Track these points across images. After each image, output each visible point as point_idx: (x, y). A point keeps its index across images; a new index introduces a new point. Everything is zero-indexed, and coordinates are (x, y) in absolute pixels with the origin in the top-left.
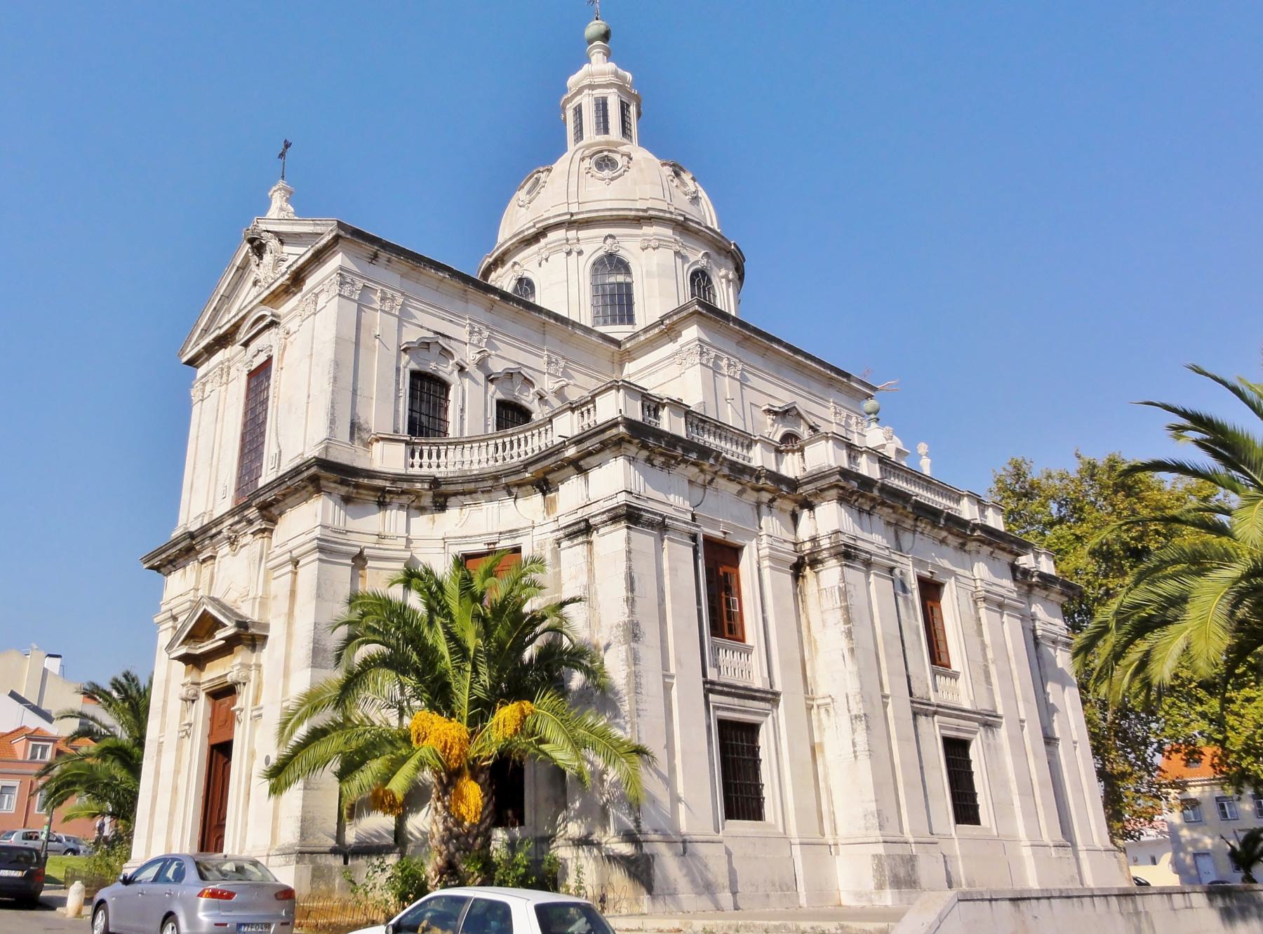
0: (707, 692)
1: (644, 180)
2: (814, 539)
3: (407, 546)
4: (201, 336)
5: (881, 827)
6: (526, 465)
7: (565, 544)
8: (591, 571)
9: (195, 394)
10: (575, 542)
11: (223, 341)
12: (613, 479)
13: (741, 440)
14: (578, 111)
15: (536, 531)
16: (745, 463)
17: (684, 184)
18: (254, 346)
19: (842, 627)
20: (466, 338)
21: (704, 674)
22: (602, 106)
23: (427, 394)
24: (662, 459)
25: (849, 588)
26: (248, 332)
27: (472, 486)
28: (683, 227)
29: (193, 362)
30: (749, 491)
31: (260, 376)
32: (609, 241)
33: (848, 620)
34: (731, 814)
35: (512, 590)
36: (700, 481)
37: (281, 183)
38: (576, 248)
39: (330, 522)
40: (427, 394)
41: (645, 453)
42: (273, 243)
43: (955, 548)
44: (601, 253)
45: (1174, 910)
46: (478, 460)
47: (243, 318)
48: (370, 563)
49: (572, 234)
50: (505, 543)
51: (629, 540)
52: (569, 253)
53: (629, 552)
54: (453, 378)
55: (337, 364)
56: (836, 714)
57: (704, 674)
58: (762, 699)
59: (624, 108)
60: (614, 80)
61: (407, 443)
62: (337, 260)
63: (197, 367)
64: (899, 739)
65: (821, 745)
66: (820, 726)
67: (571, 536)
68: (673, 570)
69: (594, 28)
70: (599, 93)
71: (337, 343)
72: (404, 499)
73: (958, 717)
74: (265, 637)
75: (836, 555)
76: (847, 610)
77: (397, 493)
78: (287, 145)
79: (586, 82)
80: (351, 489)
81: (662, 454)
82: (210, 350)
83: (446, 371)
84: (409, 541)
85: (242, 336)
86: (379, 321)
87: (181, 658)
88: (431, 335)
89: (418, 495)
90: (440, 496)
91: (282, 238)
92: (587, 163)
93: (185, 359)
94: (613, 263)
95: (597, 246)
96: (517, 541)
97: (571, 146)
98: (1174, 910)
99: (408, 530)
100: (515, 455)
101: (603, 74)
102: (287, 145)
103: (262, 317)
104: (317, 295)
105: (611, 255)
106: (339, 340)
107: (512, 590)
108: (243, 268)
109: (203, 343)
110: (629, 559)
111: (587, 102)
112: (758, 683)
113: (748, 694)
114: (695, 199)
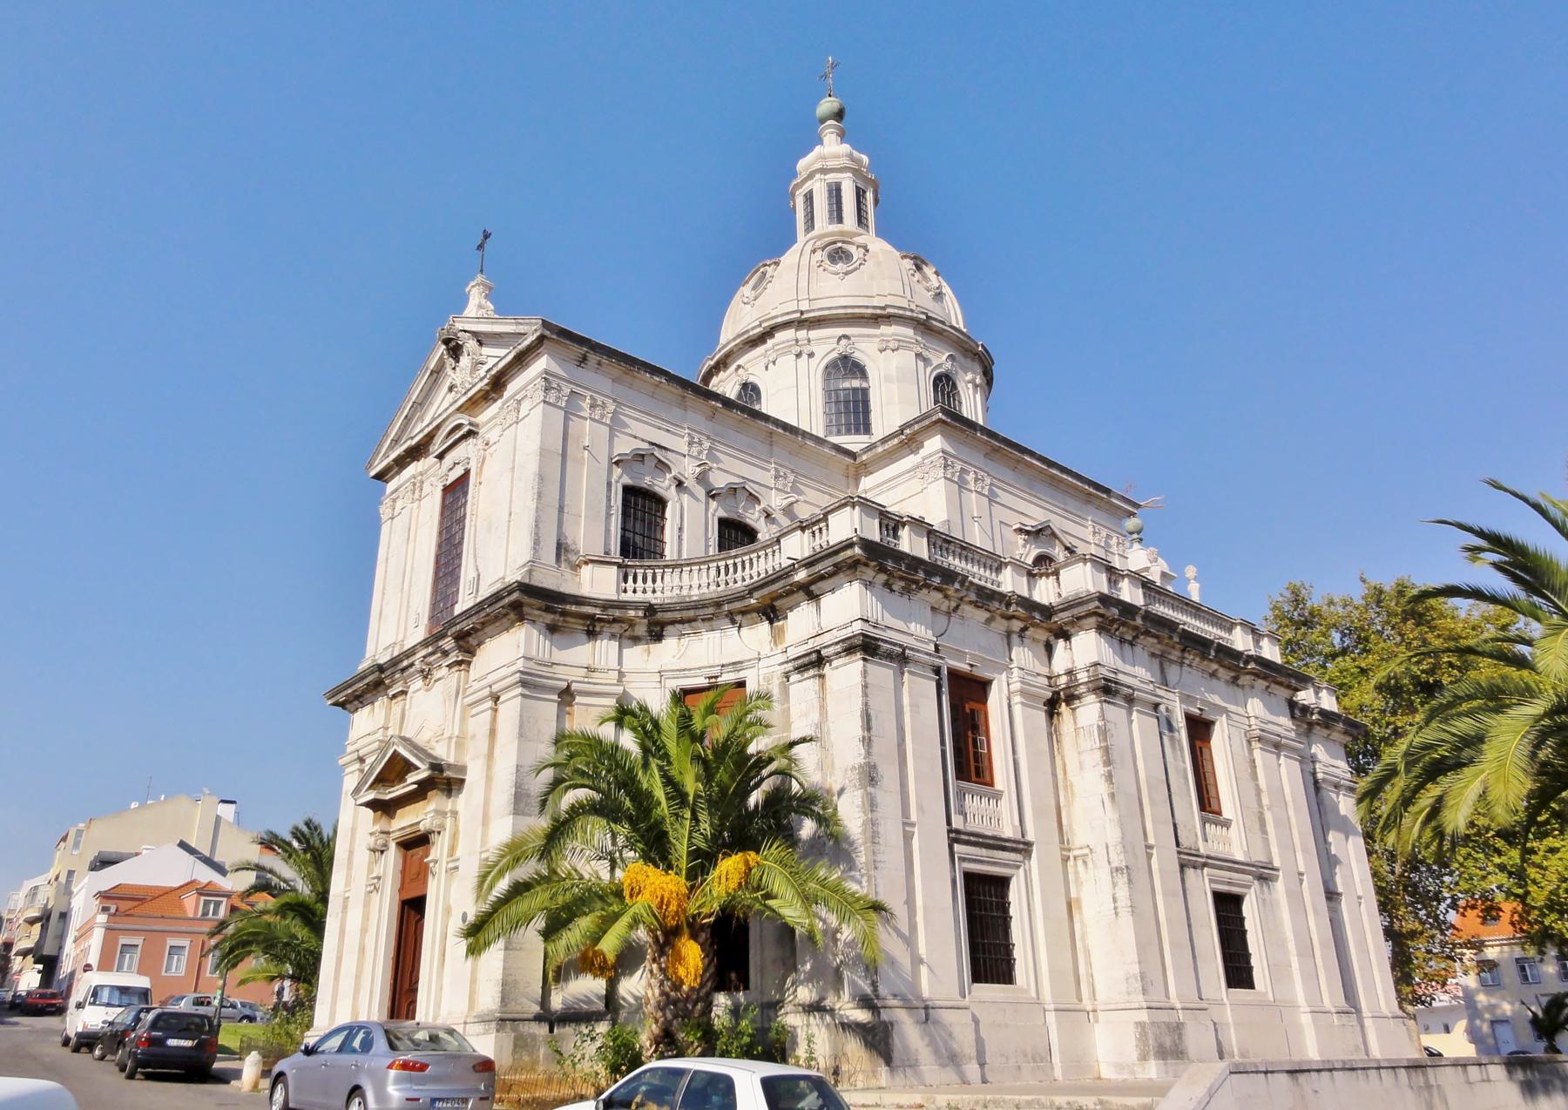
0: (952, 842)
1: (883, 274)
2: (1070, 673)
3: (620, 680)
4: (391, 448)
5: (1144, 991)
6: (752, 590)
7: (794, 677)
8: (823, 708)
9: (385, 512)
10: (806, 675)
11: (415, 453)
13: (989, 562)
14: (809, 198)
15: (763, 663)
17: (926, 278)
19: (1102, 770)
20: (685, 450)
21: (949, 822)
22: (835, 192)
23: (641, 512)
24: (902, 584)
25: (1109, 726)
26: (443, 442)
27: (691, 613)
28: (926, 326)
29: (382, 476)
30: (999, 619)
31: (456, 490)
32: (844, 342)
33: (1108, 762)
35: (735, 729)
36: (944, 608)
37: (480, 278)
38: (806, 350)
40: (641, 512)
41: (883, 577)
42: (471, 344)
43: (1227, 682)
44: (835, 355)
46: (697, 585)
47: (438, 427)
48: (578, 699)
49: (802, 334)
50: (728, 677)
51: (865, 673)
52: (798, 355)
53: (865, 686)
54: (670, 494)
55: (541, 478)
56: (1095, 866)
57: (949, 822)
59: (860, 194)
61: (619, 566)
62: (542, 363)
63: (387, 482)
64: (1164, 894)
65: (1078, 900)
67: (801, 669)
69: (827, 105)
72: (616, 628)
73: (1229, 869)
74: (462, 781)
75: (1095, 690)
76: (1106, 750)
77: (608, 622)
78: (487, 236)
79: (818, 166)
80: (557, 617)
81: (901, 578)
82: (401, 463)
83: (663, 486)
84: (621, 674)
85: (436, 447)
86: (588, 430)
88: (646, 446)
89: (631, 623)
91: (481, 339)
93: (373, 473)
94: (848, 366)
96: (741, 675)
97: (801, 237)
99: (620, 663)
100: (739, 578)
101: (837, 157)
102: (487, 236)
103: (459, 427)
104: (519, 402)
105: (845, 357)
106: (544, 452)
107: (735, 729)
108: (438, 372)
109: (393, 455)
110: (865, 695)
112: (1008, 832)
113: (998, 844)
114: (939, 296)
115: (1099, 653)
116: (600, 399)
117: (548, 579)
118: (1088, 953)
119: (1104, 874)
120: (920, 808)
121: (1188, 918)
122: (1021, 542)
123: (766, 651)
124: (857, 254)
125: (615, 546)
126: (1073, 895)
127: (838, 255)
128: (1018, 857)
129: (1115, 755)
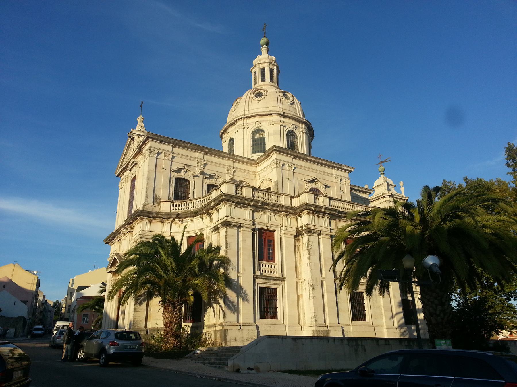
2: (301, 227)
5: (316, 321)
6: (204, 208)
7: (213, 233)
9: (120, 186)
11: (124, 170)
12: (224, 212)
13: (277, 195)
14: (256, 72)
16: (279, 203)
18: (133, 171)
19: (308, 256)
20: (196, 165)
22: (263, 71)
25: (310, 243)
29: (118, 176)
31: (133, 180)
33: (309, 254)
34: (354, 319)
37: (141, 116)
39: (145, 229)
42: (136, 137)
44: (255, 128)
45: (378, 345)
49: (245, 121)
51: (226, 232)
53: (226, 236)
55: (148, 179)
58: (278, 280)
60: (267, 60)
62: (150, 144)
64: (327, 292)
65: (302, 295)
66: (302, 289)
68: (244, 241)
70: (262, 66)
71: (148, 172)
75: (306, 232)
76: (309, 250)
83: (189, 176)
85: (129, 168)
86: (164, 162)
87: (110, 272)
90: (180, 217)
91: (139, 136)
92: (252, 95)
95: (253, 125)
98: (378, 345)
100: (185, 208)
106: (149, 171)
108: (129, 145)
110: (226, 238)
111: (258, 69)
112: (278, 275)
113: (274, 279)
115: (308, 220)
116: (167, 153)
117: (150, 208)
118: (304, 310)
119: (307, 286)
120: (244, 269)
121: (337, 300)
122: (306, 185)
123: (209, 225)
124: (264, 93)
125: (172, 196)
126: (300, 293)
127: (259, 95)
128: (280, 282)
129: (311, 251)
